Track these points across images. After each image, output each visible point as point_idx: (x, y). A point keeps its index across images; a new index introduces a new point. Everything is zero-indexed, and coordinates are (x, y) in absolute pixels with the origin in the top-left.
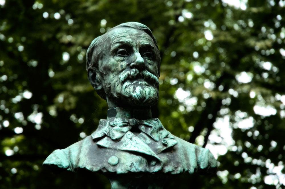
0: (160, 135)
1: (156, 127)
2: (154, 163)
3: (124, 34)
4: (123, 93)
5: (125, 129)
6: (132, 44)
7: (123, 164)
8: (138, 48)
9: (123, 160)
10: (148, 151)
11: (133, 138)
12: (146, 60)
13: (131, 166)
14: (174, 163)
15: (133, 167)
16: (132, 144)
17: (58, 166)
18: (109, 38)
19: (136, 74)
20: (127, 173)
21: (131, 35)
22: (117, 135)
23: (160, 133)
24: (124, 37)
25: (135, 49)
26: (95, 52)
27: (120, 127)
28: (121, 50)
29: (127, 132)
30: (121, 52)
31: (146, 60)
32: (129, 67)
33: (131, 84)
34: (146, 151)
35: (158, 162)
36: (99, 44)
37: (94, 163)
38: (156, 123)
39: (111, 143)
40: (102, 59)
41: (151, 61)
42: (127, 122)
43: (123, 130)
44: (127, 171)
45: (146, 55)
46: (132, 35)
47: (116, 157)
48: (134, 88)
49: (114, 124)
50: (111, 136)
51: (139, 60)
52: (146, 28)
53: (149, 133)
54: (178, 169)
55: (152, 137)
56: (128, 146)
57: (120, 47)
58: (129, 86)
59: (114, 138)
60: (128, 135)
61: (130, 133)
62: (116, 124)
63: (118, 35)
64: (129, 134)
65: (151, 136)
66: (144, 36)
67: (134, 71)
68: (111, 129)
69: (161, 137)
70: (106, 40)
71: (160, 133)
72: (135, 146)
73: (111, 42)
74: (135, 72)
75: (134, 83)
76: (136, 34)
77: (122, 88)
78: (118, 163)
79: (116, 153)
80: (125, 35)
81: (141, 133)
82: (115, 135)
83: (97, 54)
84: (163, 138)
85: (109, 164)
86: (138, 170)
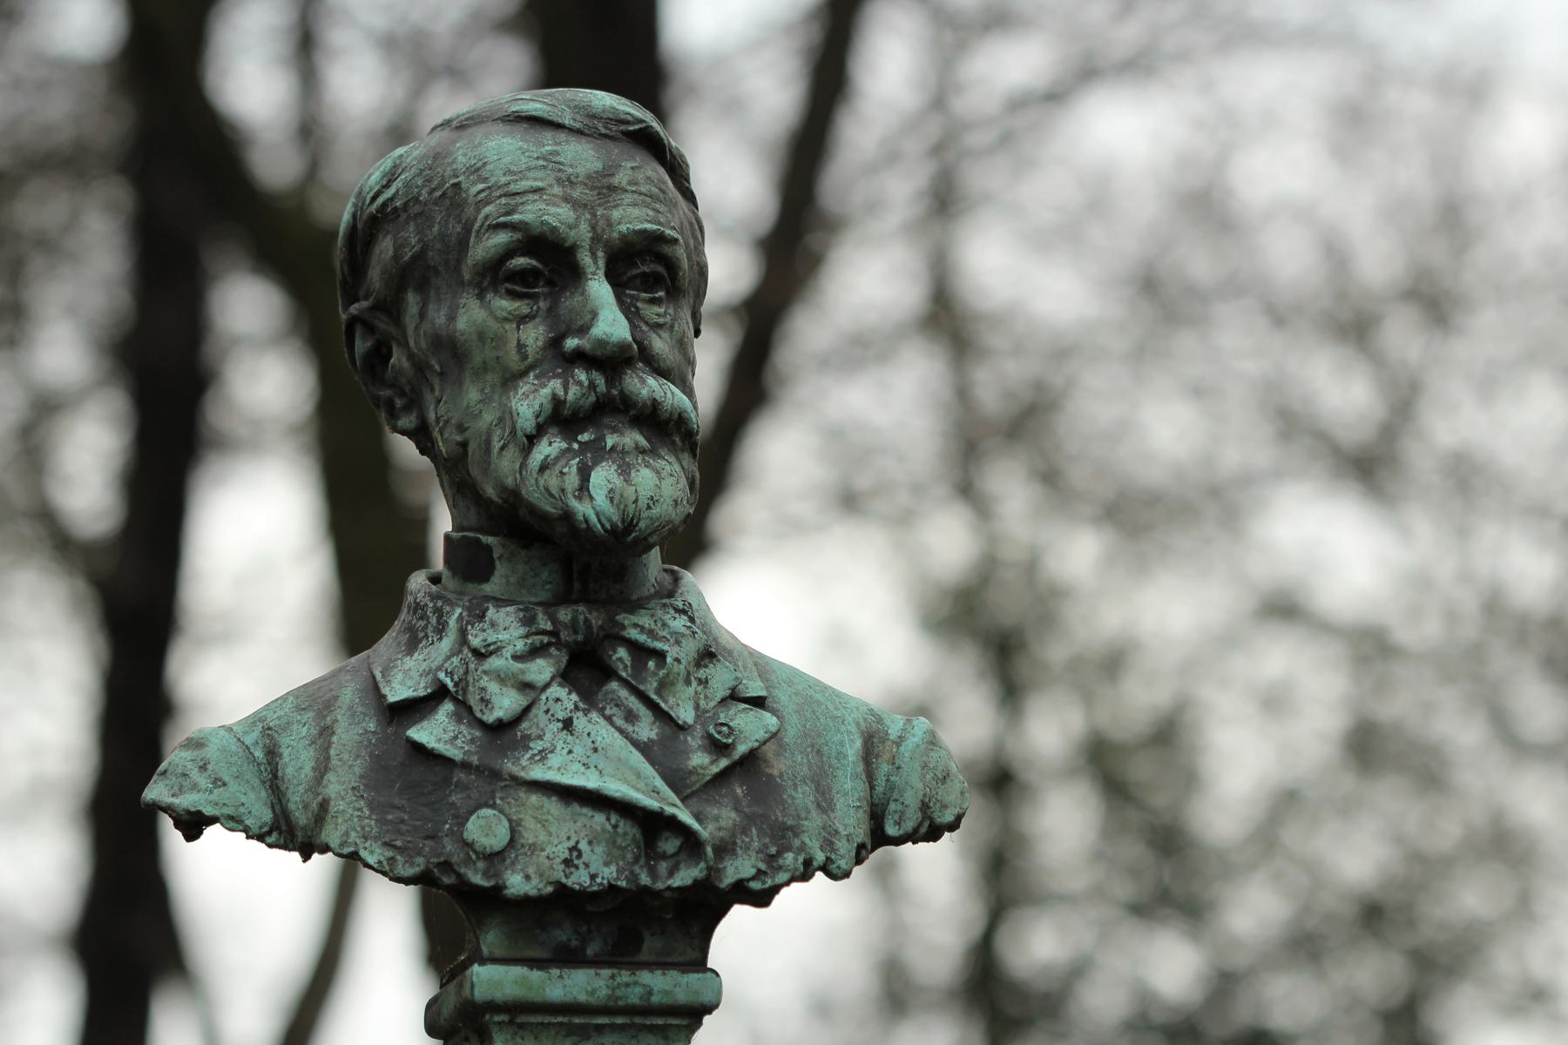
0: (700, 689)
1: (682, 656)
2: (670, 845)
4: (532, 493)
5: (541, 670)
6: (572, 233)
7: (534, 848)
8: (600, 254)
9: (531, 832)
10: (639, 784)
11: (575, 722)
13: (567, 862)
14: (761, 833)
15: (577, 867)
16: (570, 752)
18: (457, 185)
19: (592, 399)
20: (551, 895)
21: (569, 179)
22: (505, 703)
23: (700, 681)
24: (531, 197)
25: (585, 259)
26: (385, 247)
27: (516, 657)
28: (521, 261)
29: (547, 686)
30: (523, 276)
31: (639, 305)
32: (563, 359)
33: (569, 450)
34: (637, 790)
35: (691, 843)
36: (406, 204)
37: (399, 832)
38: (683, 630)
39: (472, 741)
40: (423, 287)
41: (662, 310)
42: (549, 627)
44: (550, 883)
45: (638, 281)
46: (570, 182)
47: (501, 811)
48: (585, 473)
50: (473, 700)
51: (608, 330)
53: (650, 688)
54: (781, 861)
55: (663, 705)
56: (555, 760)
57: (509, 253)
58: (557, 459)
59: (490, 718)
60: (551, 702)
61: (556, 691)
63: (503, 180)
64: (558, 700)
65: (659, 701)
66: (630, 183)
67: (580, 383)
68: (472, 666)
69: (706, 697)
70: (444, 194)
72: (584, 760)
73: (470, 211)
75: (579, 443)
76: (589, 177)
77: (523, 466)
78: (512, 842)
79: (498, 795)
80: (540, 184)
81: (614, 685)
82: (494, 699)
83: (396, 257)
84: (712, 704)
85: (469, 845)
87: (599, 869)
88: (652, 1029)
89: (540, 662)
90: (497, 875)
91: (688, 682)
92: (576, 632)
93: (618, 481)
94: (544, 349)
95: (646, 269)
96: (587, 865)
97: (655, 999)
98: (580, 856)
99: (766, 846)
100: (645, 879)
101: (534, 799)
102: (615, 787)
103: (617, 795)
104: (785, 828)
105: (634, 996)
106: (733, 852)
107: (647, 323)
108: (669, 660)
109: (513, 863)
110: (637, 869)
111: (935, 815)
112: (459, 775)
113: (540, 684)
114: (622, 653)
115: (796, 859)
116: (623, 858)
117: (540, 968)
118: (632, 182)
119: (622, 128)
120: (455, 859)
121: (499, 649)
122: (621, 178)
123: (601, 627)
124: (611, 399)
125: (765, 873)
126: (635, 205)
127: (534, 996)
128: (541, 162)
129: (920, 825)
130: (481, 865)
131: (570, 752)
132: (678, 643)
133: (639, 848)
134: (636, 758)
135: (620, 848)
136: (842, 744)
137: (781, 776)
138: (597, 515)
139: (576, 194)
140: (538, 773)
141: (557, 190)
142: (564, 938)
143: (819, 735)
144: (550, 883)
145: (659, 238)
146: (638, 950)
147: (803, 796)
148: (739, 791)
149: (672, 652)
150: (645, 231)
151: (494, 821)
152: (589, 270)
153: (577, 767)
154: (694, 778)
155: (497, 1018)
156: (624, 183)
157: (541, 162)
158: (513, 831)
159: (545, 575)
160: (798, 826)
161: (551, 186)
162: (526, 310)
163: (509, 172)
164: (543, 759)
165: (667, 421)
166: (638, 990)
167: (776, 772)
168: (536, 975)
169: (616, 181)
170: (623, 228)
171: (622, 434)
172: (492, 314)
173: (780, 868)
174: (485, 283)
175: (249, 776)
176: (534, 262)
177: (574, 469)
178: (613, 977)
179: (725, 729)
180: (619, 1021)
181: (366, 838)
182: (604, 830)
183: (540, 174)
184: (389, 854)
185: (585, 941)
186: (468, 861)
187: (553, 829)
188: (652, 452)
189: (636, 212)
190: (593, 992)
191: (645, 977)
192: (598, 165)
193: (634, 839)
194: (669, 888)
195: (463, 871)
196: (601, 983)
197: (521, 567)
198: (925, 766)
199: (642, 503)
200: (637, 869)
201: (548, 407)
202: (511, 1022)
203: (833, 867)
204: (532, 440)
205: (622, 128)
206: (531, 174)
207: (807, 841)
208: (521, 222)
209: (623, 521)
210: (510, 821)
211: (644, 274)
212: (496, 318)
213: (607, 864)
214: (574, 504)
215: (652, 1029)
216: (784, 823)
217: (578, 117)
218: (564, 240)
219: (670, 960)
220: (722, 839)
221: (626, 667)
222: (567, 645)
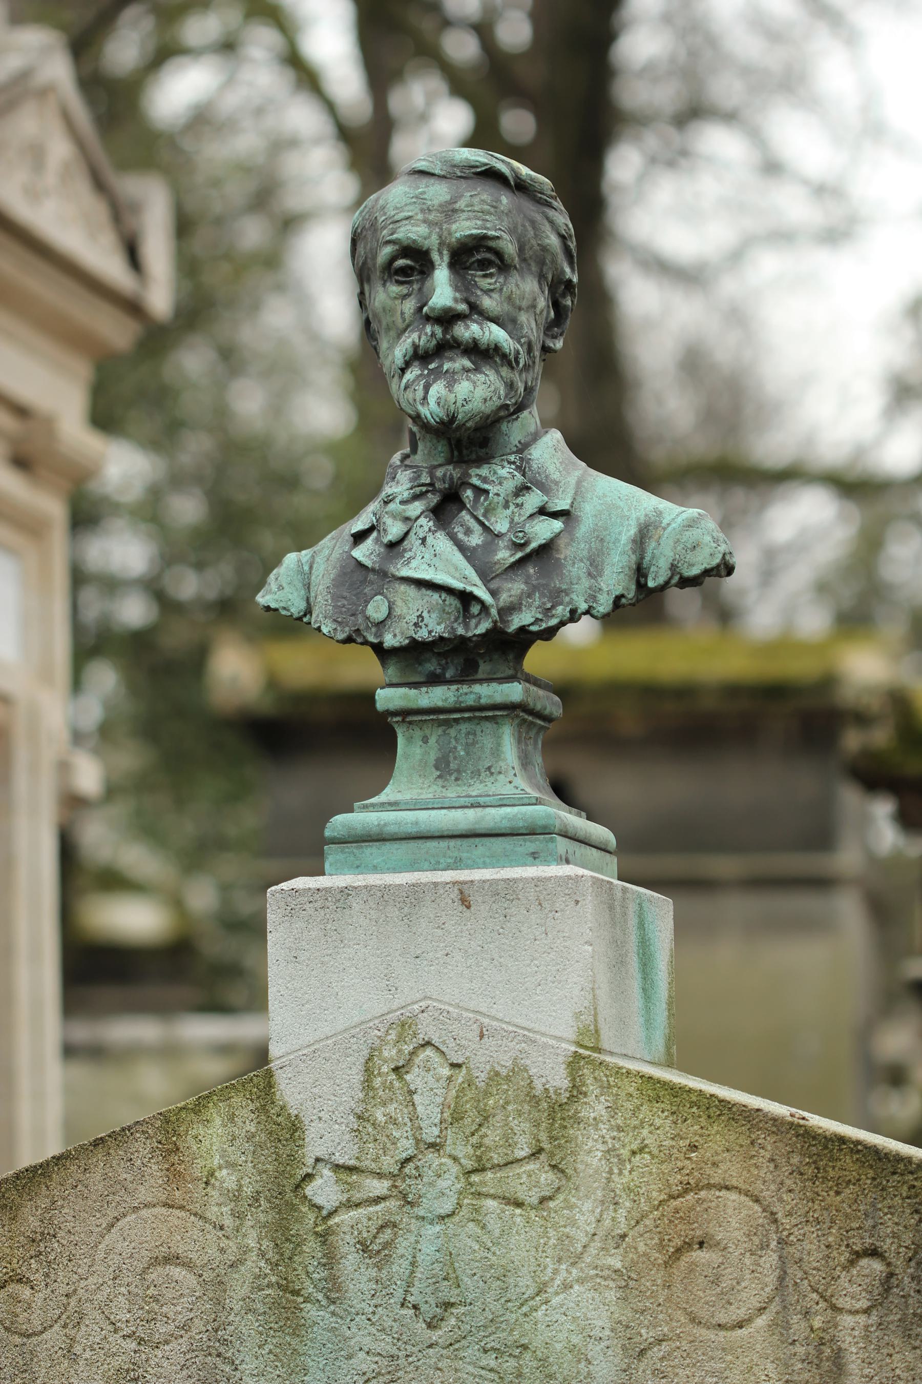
5: (417, 508)
6: (426, 242)
8: (445, 252)
13: (416, 625)
14: (542, 595)
19: (434, 342)
23: (517, 505)
24: (405, 222)
25: (435, 256)
30: (403, 271)
31: (477, 279)
33: (421, 375)
34: (454, 577)
37: (341, 613)
41: (493, 281)
43: (408, 514)
45: (476, 265)
47: (386, 597)
48: (427, 388)
52: (483, 169)
53: (480, 513)
54: (554, 612)
55: (486, 523)
58: (414, 381)
61: (423, 521)
63: (393, 213)
66: (467, 206)
69: (520, 514)
71: (517, 505)
74: (432, 335)
76: (441, 205)
80: (410, 214)
84: (523, 519)
85: (368, 618)
86: (433, 634)
87: (435, 627)
88: (487, 718)
89: (417, 503)
90: (381, 636)
91: (506, 506)
94: (414, 314)
96: (426, 626)
98: (422, 621)
99: (544, 604)
100: (460, 631)
101: (403, 588)
102: (441, 578)
105: (470, 701)
106: (520, 609)
107: (482, 290)
110: (455, 625)
112: (371, 576)
113: (413, 518)
114: (469, 493)
116: (449, 619)
117: (415, 688)
119: (473, 170)
120: (361, 628)
121: (394, 498)
122: (461, 204)
124: (448, 341)
125: (541, 620)
126: (468, 219)
128: (414, 200)
129: (671, 578)
130: (374, 630)
132: (500, 484)
135: (448, 613)
136: (620, 533)
139: (431, 217)
140: (405, 572)
141: (420, 216)
142: (432, 668)
143: (606, 529)
145: (485, 237)
146: (476, 672)
148: (532, 571)
149: (492, 489)
150: (472, 235)
151: (381, 602)
152: (437, 263)
153: (425, 566)
154: (497, 567)
155: (395, 719)
156: (462, 207)
157: (414, 200)
158: (390, 608)
159: (440, 449)
160: (569, 589)
161: (417, 214)
162: (405, 291)
163: (397, 208)
164: (409, 563)
165: (487, 350)
166: (472, 696)
167: (562, 556)
168: (413, 692)
169: (457, 206)
170: (458, 235)
171: (455, 361)
172: (388, 295)
173: (553, 616)
174: (386, 277)
175: (296, 582)
176: (408, 262)
177: (421, 387)
178: (458, 690)
181: (326, 618)
183: (411, 207)
184: (334, 626)
185: (444, 669)
186: (368, 628)
188: (477, 370)
189: (468, 223)
190: (446, 699)
191: (477, 688)
192: (448, 197)
193: (456, 607)
194: (475, 635)
195: (365, 634)
196: (451, 694)
197: (429, 444)
199: (459, 404)
200: (455, 625)
202: (403, 721)
203: (594, 612)
204: (403, 370)
205: (473, 170)
206: (407, 208)
207: (574, 596)
208: (397, 239)
209: (448, 415)
210: (389, 602)
211: (478, 261)
212: (390, 298)
213: (439, 624)
214: (420, 408)
215: (487, 718)
216: (560, 588)
219: (495, 676)
220: (512, 602)
222: (440, 491)
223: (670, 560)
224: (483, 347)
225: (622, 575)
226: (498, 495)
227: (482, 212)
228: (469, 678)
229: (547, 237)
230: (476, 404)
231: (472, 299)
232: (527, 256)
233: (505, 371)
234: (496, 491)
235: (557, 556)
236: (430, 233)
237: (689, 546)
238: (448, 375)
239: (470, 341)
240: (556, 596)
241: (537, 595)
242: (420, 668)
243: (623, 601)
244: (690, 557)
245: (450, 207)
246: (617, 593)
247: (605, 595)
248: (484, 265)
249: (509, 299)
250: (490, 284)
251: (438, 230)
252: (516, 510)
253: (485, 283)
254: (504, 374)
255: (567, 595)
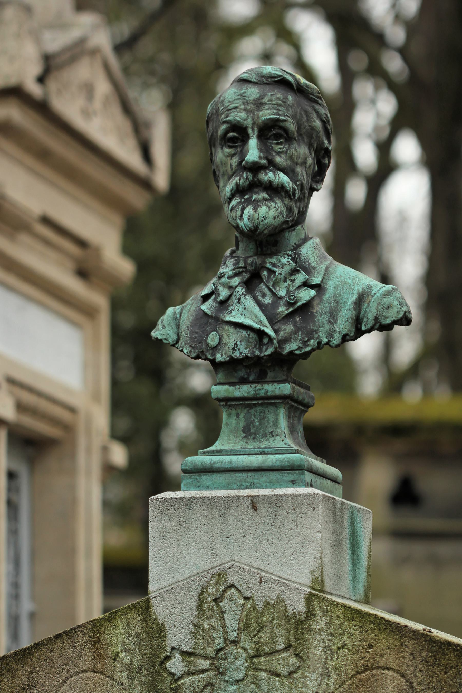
3: (236, 104)
5: (236, 281)
6: (245, 122)
8: (256, 129)
12: (272, 147)
13: (233, 349)
14: (303, 333)
17: (163, 340)
19: (248, 183)
25: (250, 131)
28: (231, 134)
29: (237, 286)
30: (233, 140)
31: (273, 146)
33: (240, 202)
34: (254, 322)
41: (282, 146)
44: (228, 356)
45: (273, 137)
47: (218, 333)
48: (243, 210)
49: (221, 274)
52: (279, 79)
54: (309, 343)
55: (274, 290)
57: (227, 132)
58: (236, 206)
61: (239, 288)
62: (223, 273)
66: (269, 101)
69: (293, 286)
71: (291, 281)
75: (245, 199)
76: (254, 100)
80: (237, 105)
84: (294, 288)
87: (244, 350)
88: (271, 404)
91: (285, 281)
92: (252, 267)
93: (252, 212)
95: (274, 132)
96: (239, 349)
97: (269, 394)
98: (237, 347)
99: (304, 338)
100: (257, 353)
102: (248, 322)
103: (247, 324)
104: (313, 331)
105: (262, 393)
108: (277, 274)
109: (219, 350)
111: (382, 321)
112: (211, 321)
115: (314, 342)
117: (233, 386)
118: (270, 100)
119: (273, 80)
121: (224, 275)
122: (265, 100)
123: (260, 264)
124: (255, 182)
125: (302, 348)
127: (231, 395)
128: (239, 97)
129: (374, 325)
131: (238, 310)
133: (257, 342)
134: (257, 310)
135: (251, 342)
137: (316, 313)
138: (244, 225)
139: (248, 107)
140: (228, 318)
142: (242, 374)
144: (228, 356)
145: (278, 120)
147: (322, 319)
148: (298, 319)
149: (278, 271)
150: (270, 118)
151: (215, 336)
152: (251, 135)
153: (239, 315)
154: (279, 316)
156: (266, 102)
157: (239, 97)
158: (220, 339)
159: (251, 246)
160: (318, 330)
161: (240, 105)
162: (233, 152)
165: (277, 188)
166: (263, 391)
167: (315, 311)
168: (231, 388)
169: (263, 101)
170: (263, 118)
171: (259, 195)
173: (308, 345)
175: (172, 324)
176: (235, 134)
179: (292, 297)
180: (260, 402)
181: (186, 344)
182: (245, 337)
183: (237, 101)
184: (190, 349)
185: (249, 375)
186: (208, 351)
187: (231, 338)
188: (271, 200)
189: (268, 112)
190: (249, 392)
191: (266, 386)
192: (258, 96)
193: (255, 339)
194: (265, 355)
196: (252, 389)
198: (379, 304)
201: (235, 188)
202: (226, 405)
203: (331, 344)
204: (230, 199)
205: (273, 80)
206: (235, 102)
207: (320, 334)
209: (254, 226)
210: (219, 335)
211: (274, 134)
213: (246, 349)
215: (271, 404)
217: (257, 78)
218: (243, 125)
219: (276, 380)
220: (286, 337)
221: (266, 277)
222: (250, 271)
223: (375, 315)
224: (275, 186)
225: (347, 322)
226: (281, 274)
227: (277, 105)
228: (264, 380)
229: (314, 121)
230: (269, 220)
231: (270, 157)
232: (302, 132)
233: (287, 201)
234: (279, 272)
235: (312, 311)
236: (248, 117)
237: (386, 307)
238: (255, 202)
239: (268, 182)
240: (311, 334)
241: (300, 333)
242: (236, 375)
243: (348, 337)
244: (386, 313)
245: (259, 101)
246: (344, 333)
247: (338, 334)
248: (277, 137)
249: (291, 158)
250: (280, 148)
251: (252, 115)
252: (290, 283)
253: (278, 148)
254: (286, 202)
255: (317, 333)
